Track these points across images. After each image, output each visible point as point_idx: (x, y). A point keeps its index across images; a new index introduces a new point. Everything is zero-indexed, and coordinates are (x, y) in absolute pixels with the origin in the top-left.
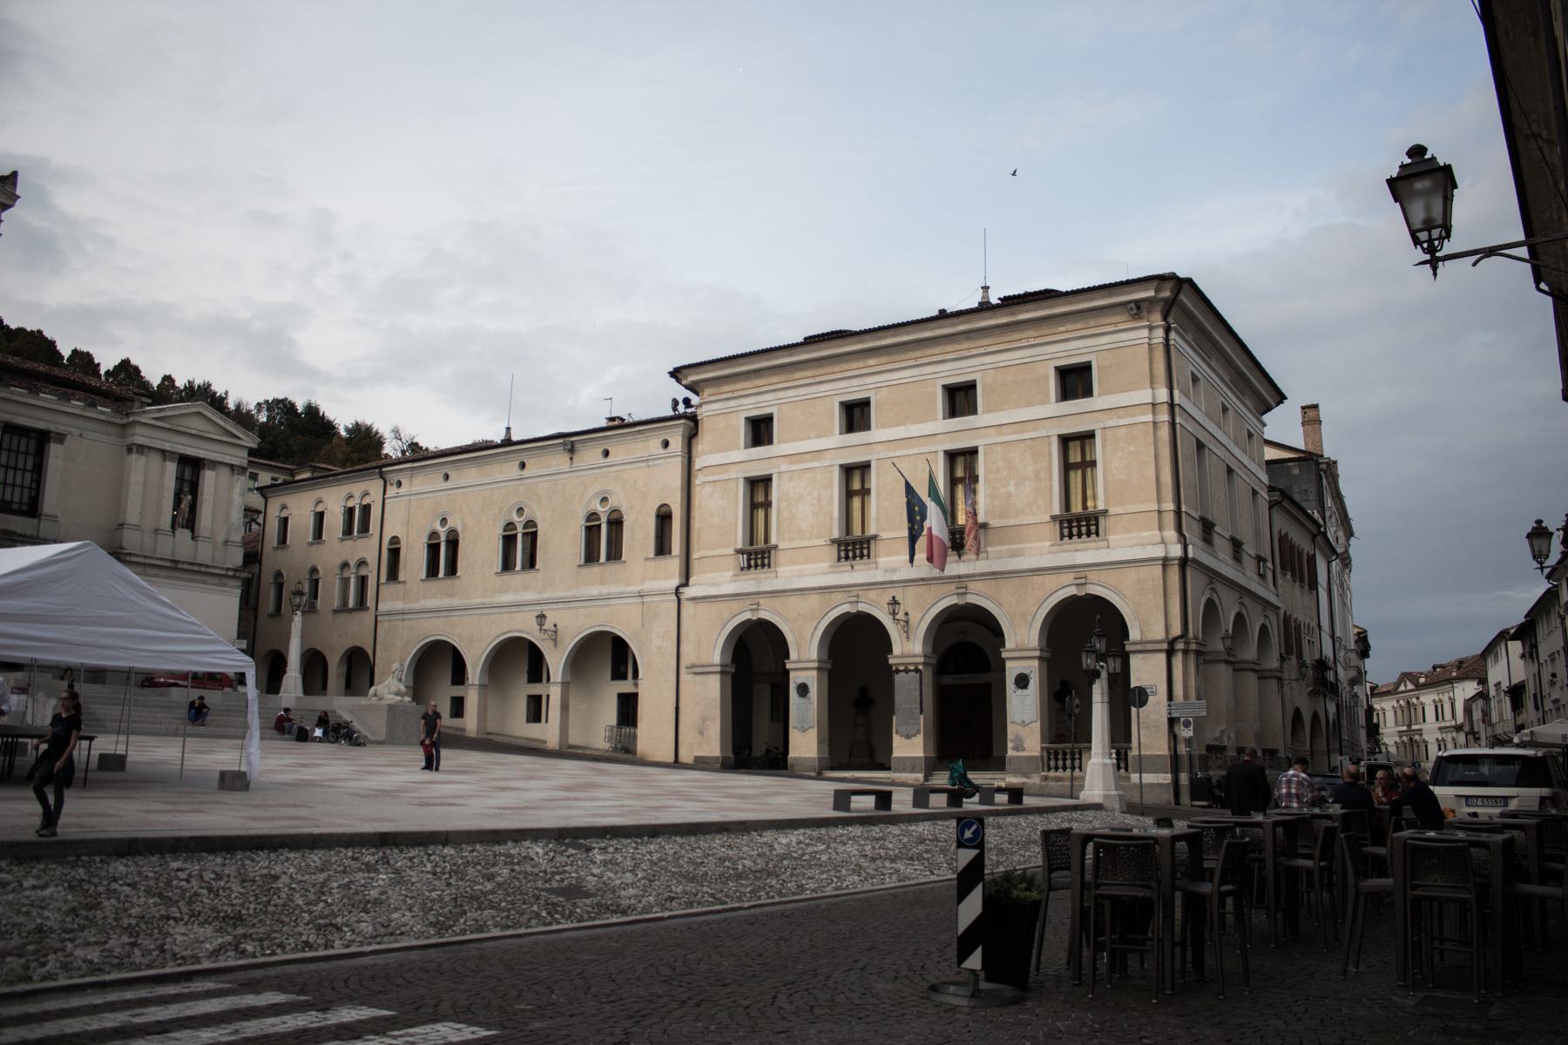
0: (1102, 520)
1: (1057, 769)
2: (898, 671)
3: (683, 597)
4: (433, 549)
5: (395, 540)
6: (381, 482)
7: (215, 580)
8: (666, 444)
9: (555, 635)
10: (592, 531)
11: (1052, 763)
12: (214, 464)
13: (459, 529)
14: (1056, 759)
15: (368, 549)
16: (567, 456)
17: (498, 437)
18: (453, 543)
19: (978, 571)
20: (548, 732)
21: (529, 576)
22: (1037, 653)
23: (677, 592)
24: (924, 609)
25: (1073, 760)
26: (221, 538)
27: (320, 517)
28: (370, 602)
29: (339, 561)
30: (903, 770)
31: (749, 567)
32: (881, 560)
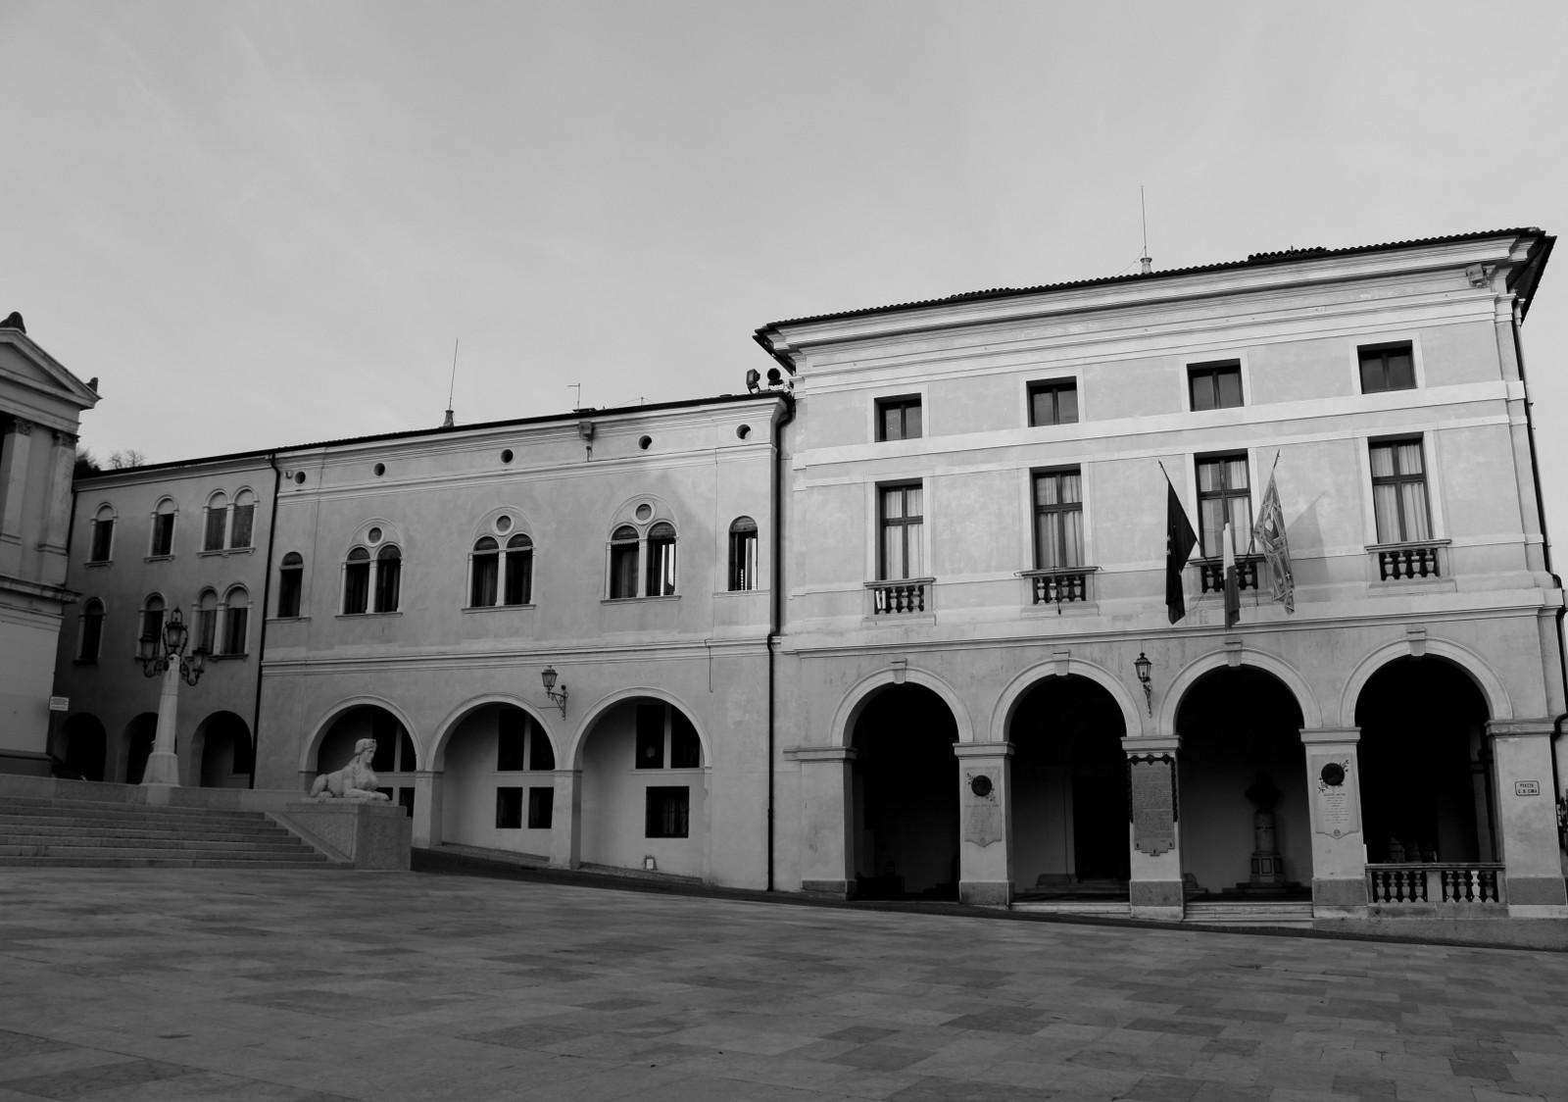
0: (1089, 579)
1: (1388, 898)
2: (1136, 760)
3: (777, 650)
4: (356, 574)
5: (294, 558)
6: (272, 474)
7: (22, 603)
8: (743, 431)
9: (564, 702)
10: (483, 564)
11: (1381, 891)
12: (29, 426)
13: (402, 545)
14: (1387, 885)
15: (251, 571)
16: (583, 444)
17: (439, 422)
18: (390, 563)
19: (1261, 620)
20: (553, 844)
21: (516, 614)
22: (1005, 750)
23: (770, 638)
24: (1187, 666)
25: (1412, 886)
26: (32, 539)
27: (166, 523)
28: (250, 645)
29: (199, 587)
30: (1150, 902)
31: (888, 609)
32: (1104, 603)
